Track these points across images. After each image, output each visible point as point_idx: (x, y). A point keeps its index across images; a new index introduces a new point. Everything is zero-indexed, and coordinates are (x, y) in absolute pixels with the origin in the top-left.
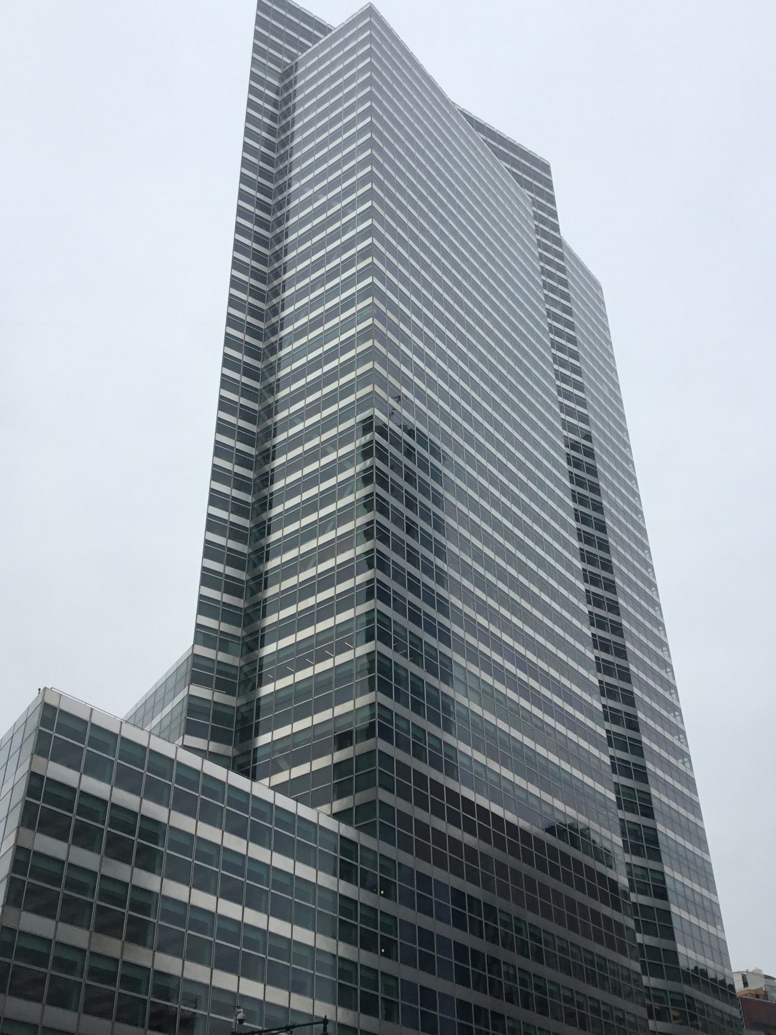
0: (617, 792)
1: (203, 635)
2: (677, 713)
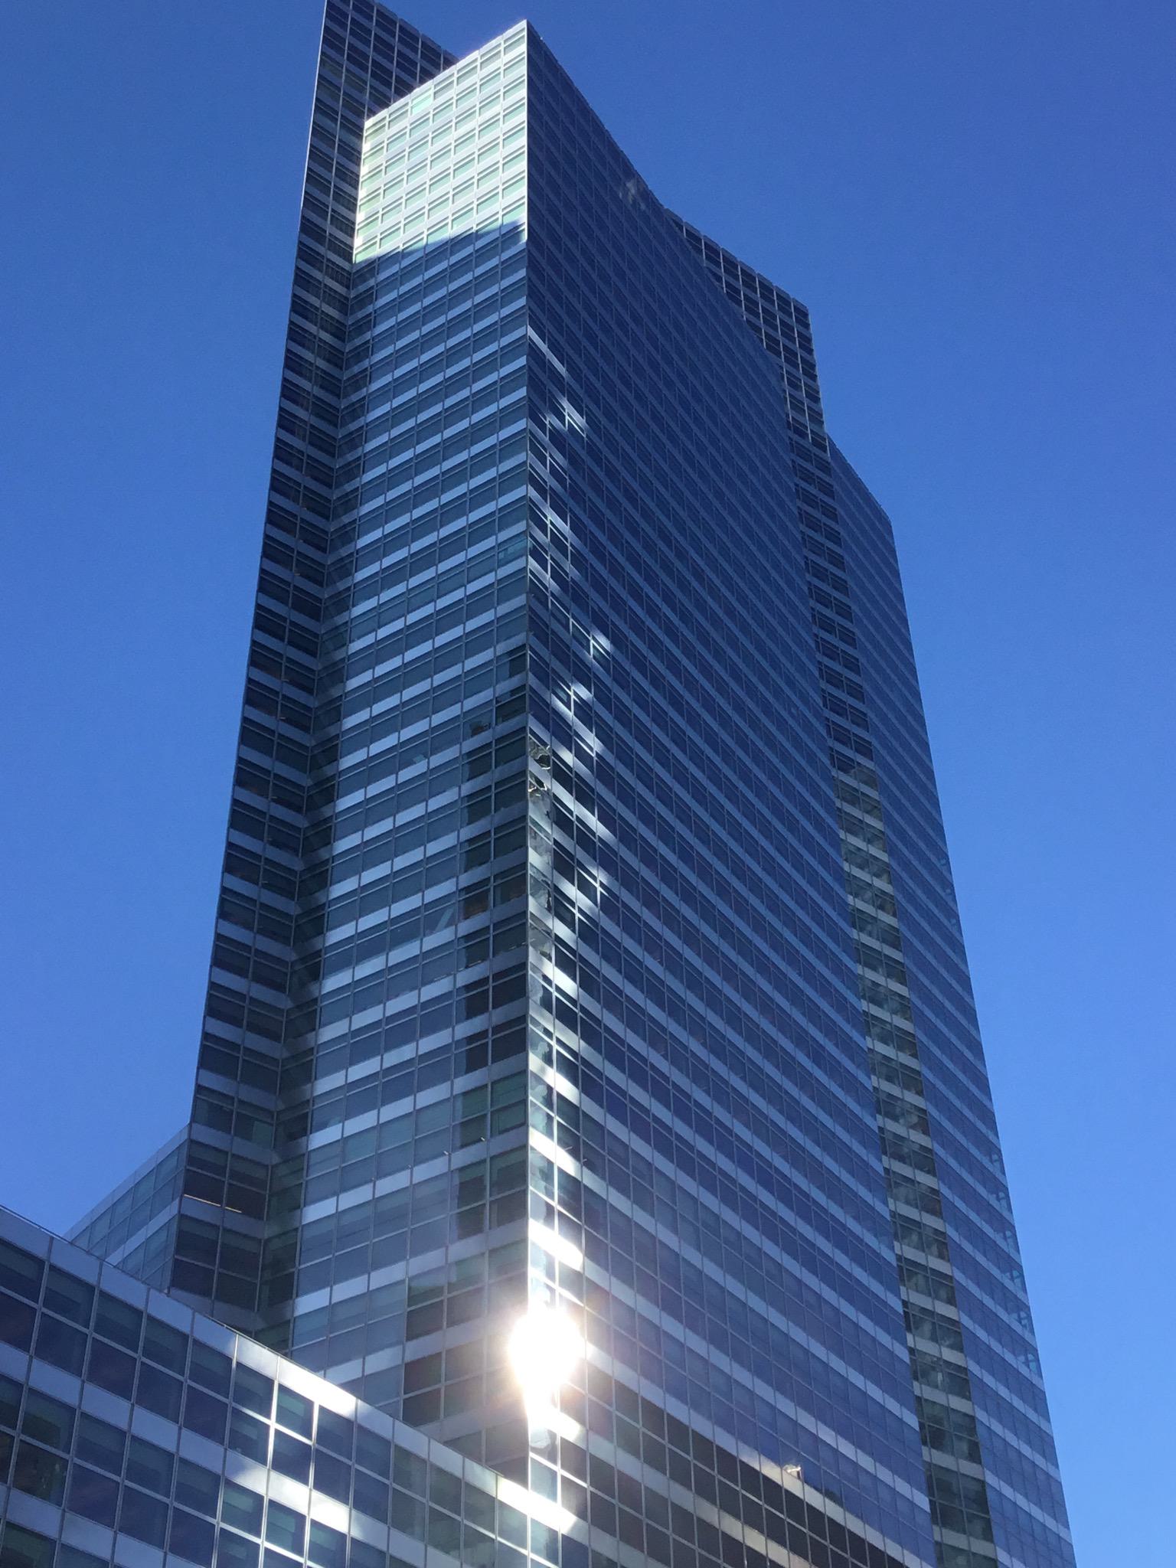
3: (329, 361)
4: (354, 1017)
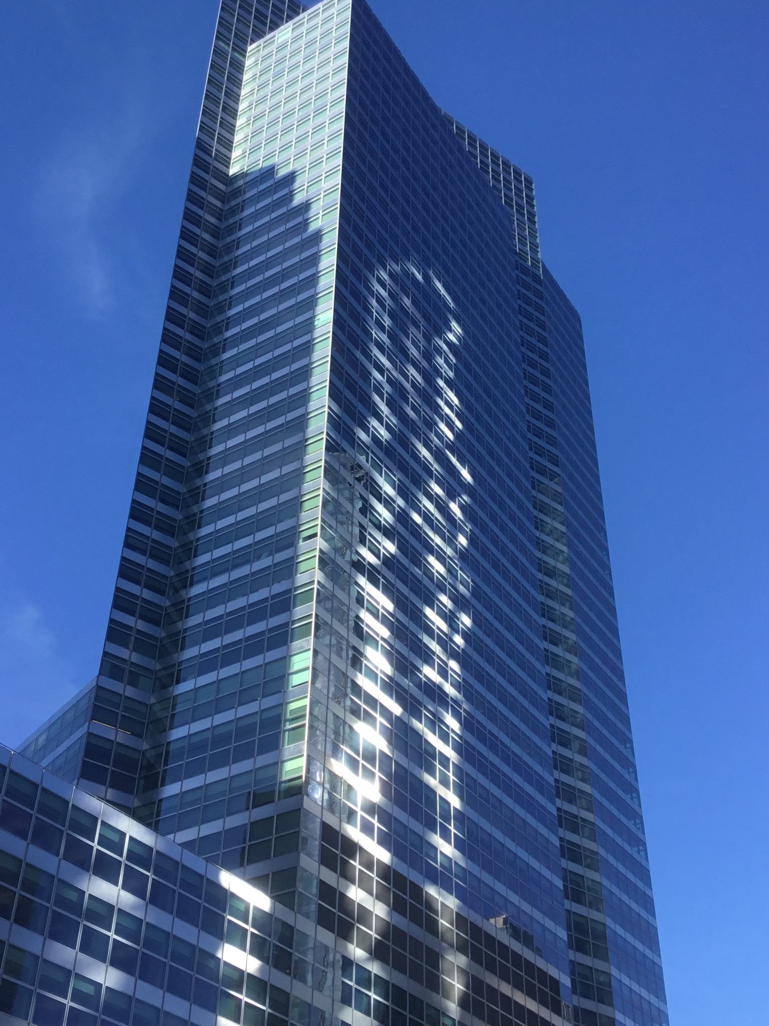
0: (565, 880)
1: (111, 666)
2: (638, 821)
3: (202, 272)
4: (207, 613)
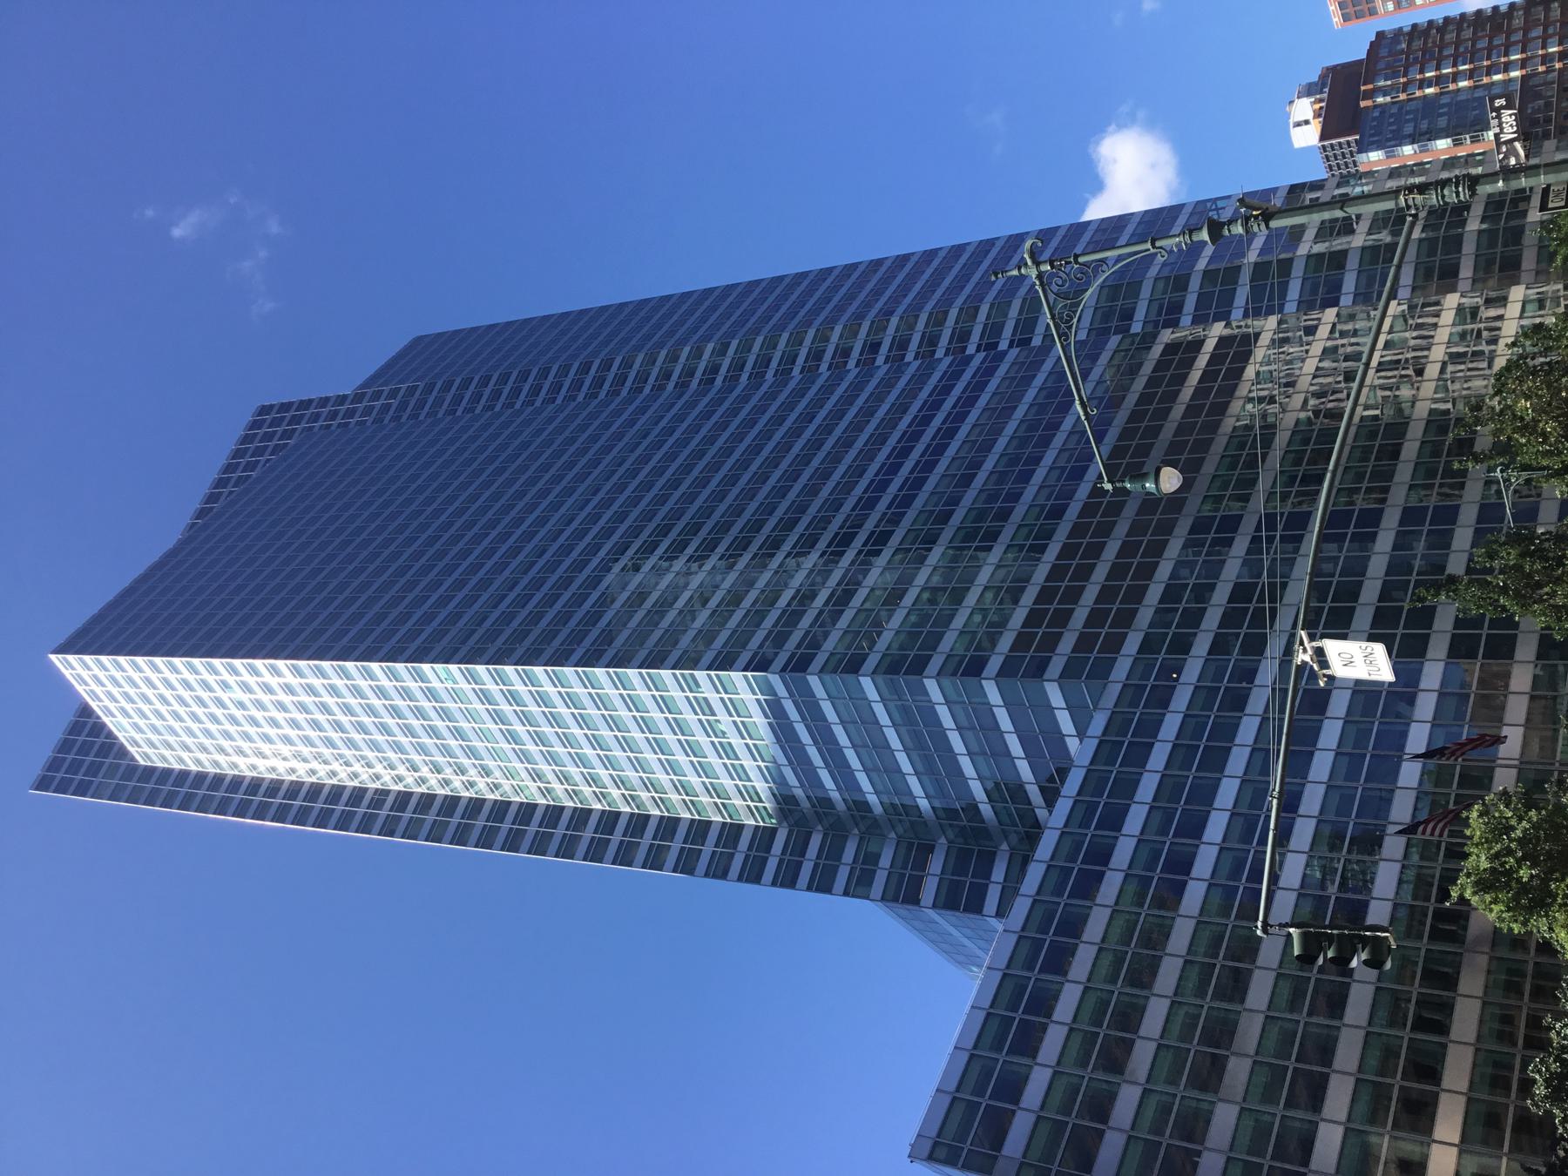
1: (859, 886)
